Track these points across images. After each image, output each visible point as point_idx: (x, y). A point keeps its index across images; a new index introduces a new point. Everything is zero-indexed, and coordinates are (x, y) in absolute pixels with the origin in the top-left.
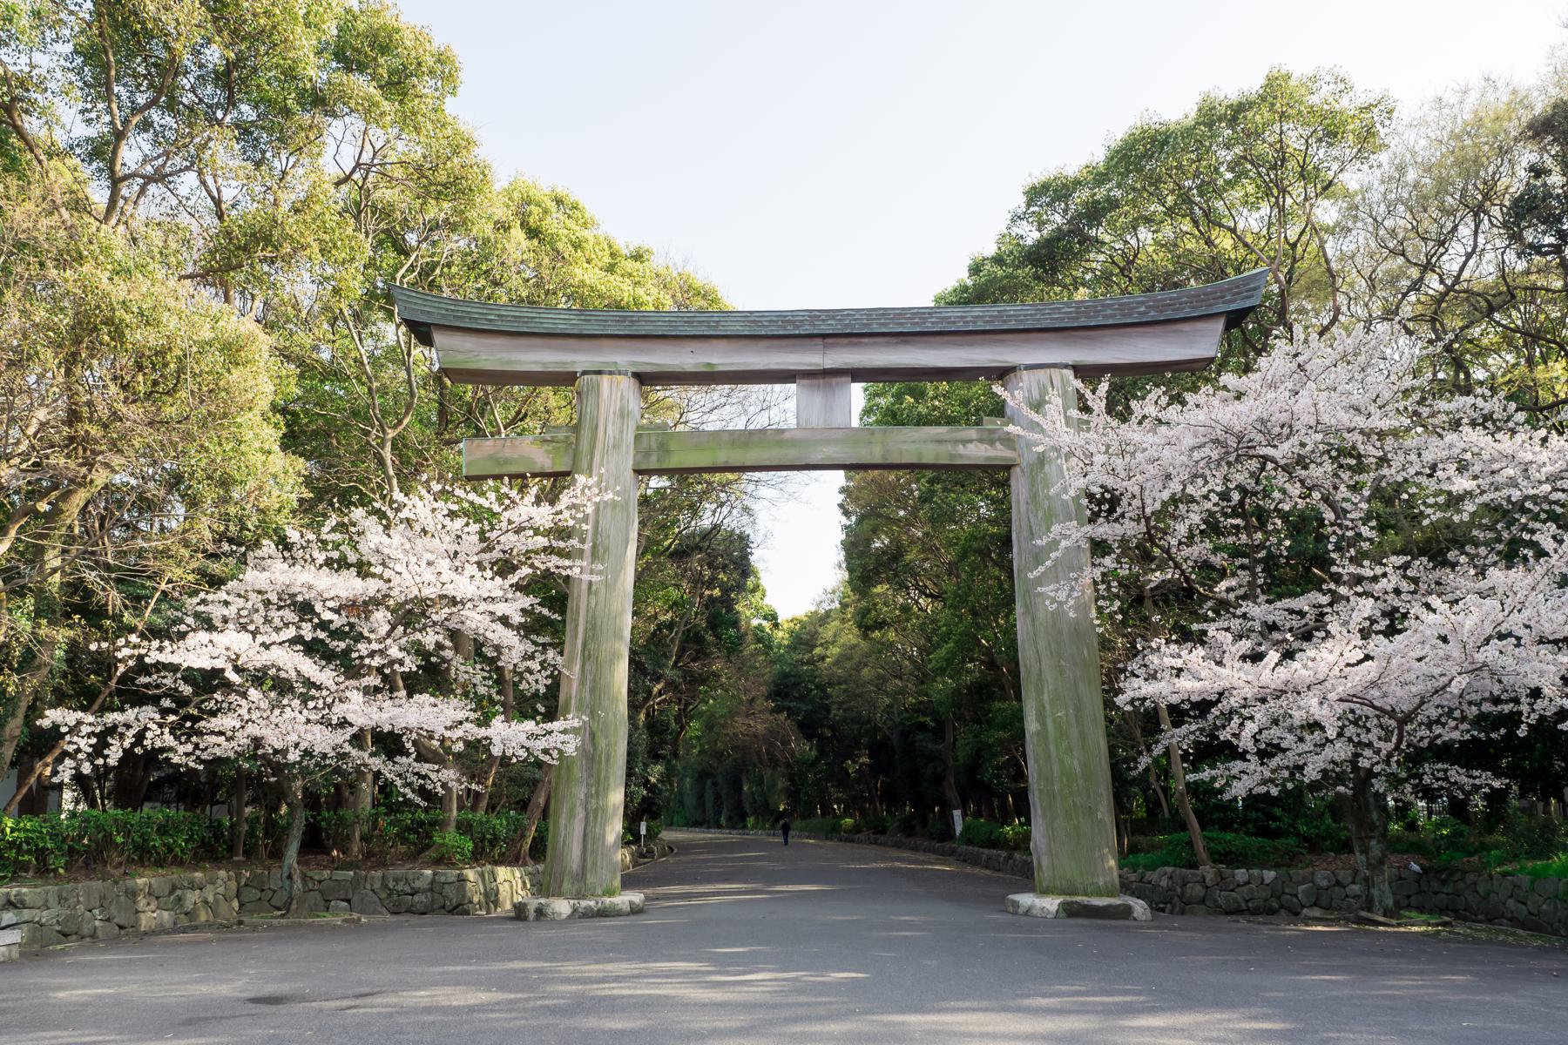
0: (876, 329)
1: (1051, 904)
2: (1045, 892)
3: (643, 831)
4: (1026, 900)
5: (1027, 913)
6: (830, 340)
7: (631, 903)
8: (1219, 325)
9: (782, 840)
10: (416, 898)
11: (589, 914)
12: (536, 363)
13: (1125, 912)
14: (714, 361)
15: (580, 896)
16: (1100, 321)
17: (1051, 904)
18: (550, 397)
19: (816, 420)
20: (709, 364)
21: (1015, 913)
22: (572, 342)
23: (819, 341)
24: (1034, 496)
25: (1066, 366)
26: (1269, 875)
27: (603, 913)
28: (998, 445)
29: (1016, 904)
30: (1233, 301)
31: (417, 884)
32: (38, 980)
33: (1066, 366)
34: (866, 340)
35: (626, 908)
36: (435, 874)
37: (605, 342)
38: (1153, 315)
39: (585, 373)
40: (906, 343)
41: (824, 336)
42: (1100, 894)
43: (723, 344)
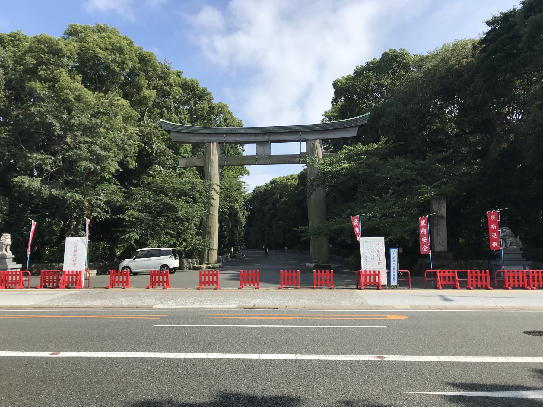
2: (312, 262)
3: (232, 250)
4: (307, 264)
15: (208, 264)
41: (256, 134)
43: (239, 135)
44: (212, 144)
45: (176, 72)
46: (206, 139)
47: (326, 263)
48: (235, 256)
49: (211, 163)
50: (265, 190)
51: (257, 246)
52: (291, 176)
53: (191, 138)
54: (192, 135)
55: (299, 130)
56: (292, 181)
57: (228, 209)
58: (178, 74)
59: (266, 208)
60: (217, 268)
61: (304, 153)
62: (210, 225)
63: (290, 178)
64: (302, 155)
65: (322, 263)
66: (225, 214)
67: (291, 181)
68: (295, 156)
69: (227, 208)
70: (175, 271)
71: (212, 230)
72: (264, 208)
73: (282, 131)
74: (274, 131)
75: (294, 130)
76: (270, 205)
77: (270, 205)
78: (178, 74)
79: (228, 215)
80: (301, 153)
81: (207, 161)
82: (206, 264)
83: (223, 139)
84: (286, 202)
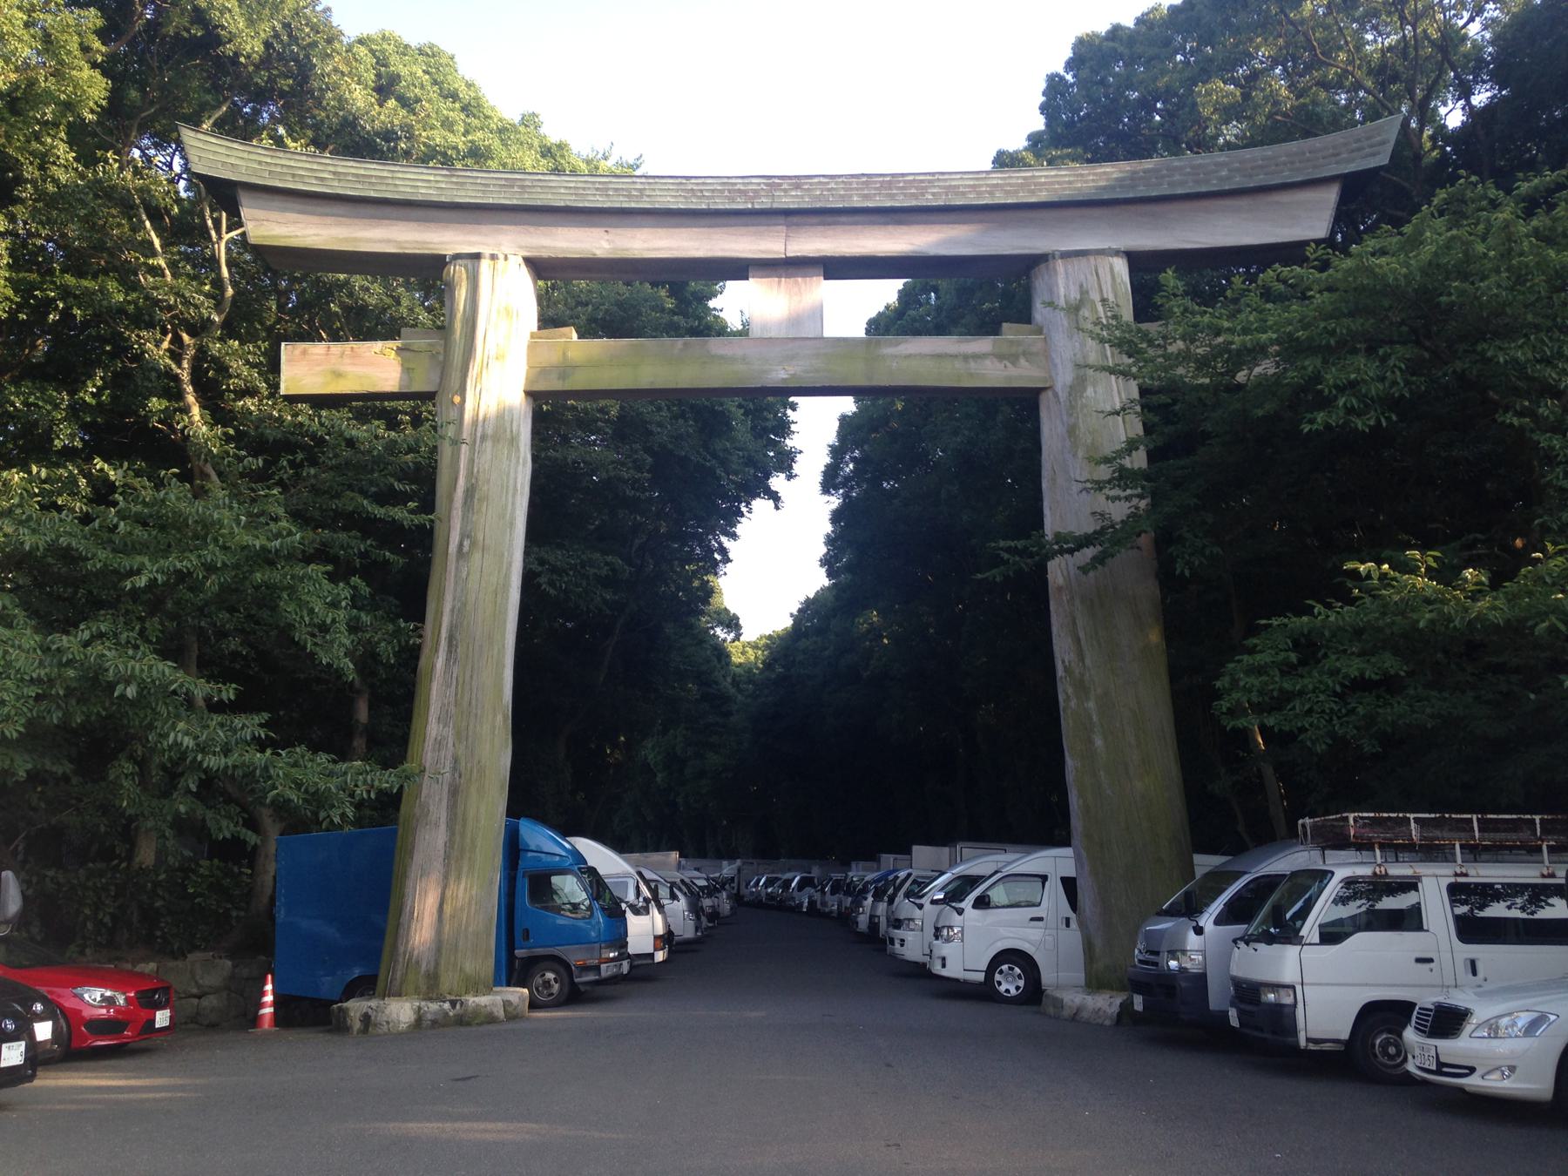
0: (857, 202)
6: (795, 219)
7: (506, 1004)
8: (1331, 195)
9: (1050, 393)
10: (205, 1002)
12: (389, 241)
16: (1165, 190)
22: (371, 210)
23: (781, 219)
24: (1072, 431)
25: (1117, 253)
28: (1022, 361)
30: (1353, 160)
32: (1012, 371)
33: (1117, 253)
34: (843, 219)
38: (1238, 182)
40: (900, 223)
41: (787, 213)
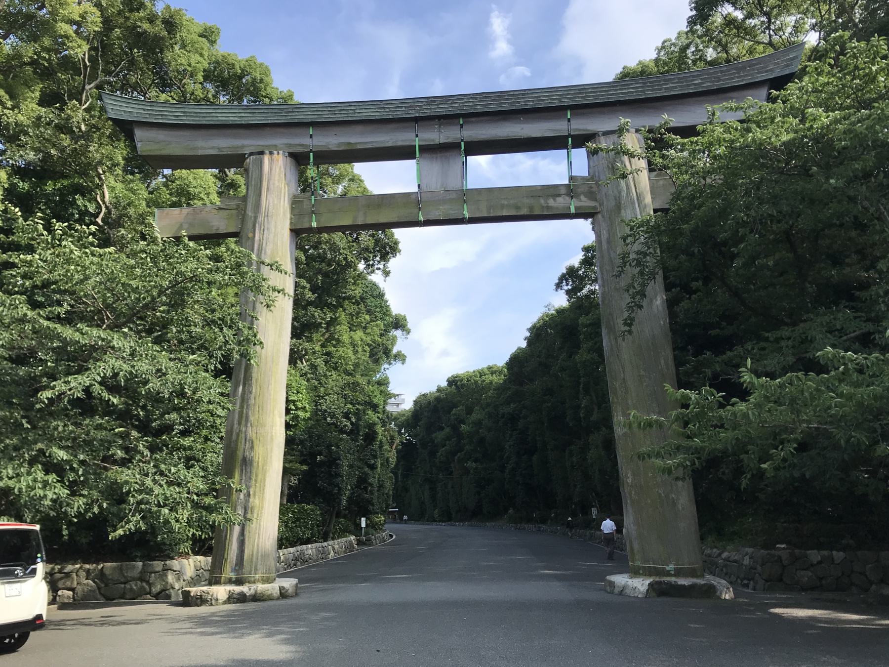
1: (640, 585)
2: (636, 573)
3: (363, 525)
4: (620, 580)
5: (621, 593)
11: (242, 598)
12: (213, 148)
13: (710, 591)
14: (353, 140)
15: (239, 582)
17: (640, 585)
18: (204, 180)
19: (434, 184)
20: (349, 144)
21: (612, 593)
26: (838, 555)
27: (256, 598)
29: (612, 584)
31: (130, 574)
35: (276, 592)
36: (144, 565)
37: (267, 130)
39: (251, 154)
40: (505, 119)
41: (416, 120)
42: (161, 617)
43: (359, 128)
44: (266, 158)
45: (200, 30)
46: (246, 143)
47: (692, 573)
48: (369, 540)
49: (261, 219)
50: (438, 399)
51: (419, 516)
52: (489, 368)
53: (200, 143)
54: (203, 132)
55: (566, 102)
56: (491, 378)
57: (349, 419)
58: (209, 35)
59: (439, 436)
60: (270, 598)
61: (583, 178)
62: (251, 433)
63: (486, 371)
64: (572, 188)
65: (678, 573)
66: (342, 431)
67: (489, 378)
68: (551, 191)
69: (346, 416)
70: (23, 638)
71: (259, 454)
72: (434, 435)
73: (506, 107)
74: (480, 109)
75: (547, 103)
76: (447, 430)
77: (447, 430)
78: (209, 35)
79: (348, 434)
80: (571, 178)
81: (250, 213)
82: (230, 581)
83: (306, 141)
84: (478, 423)
